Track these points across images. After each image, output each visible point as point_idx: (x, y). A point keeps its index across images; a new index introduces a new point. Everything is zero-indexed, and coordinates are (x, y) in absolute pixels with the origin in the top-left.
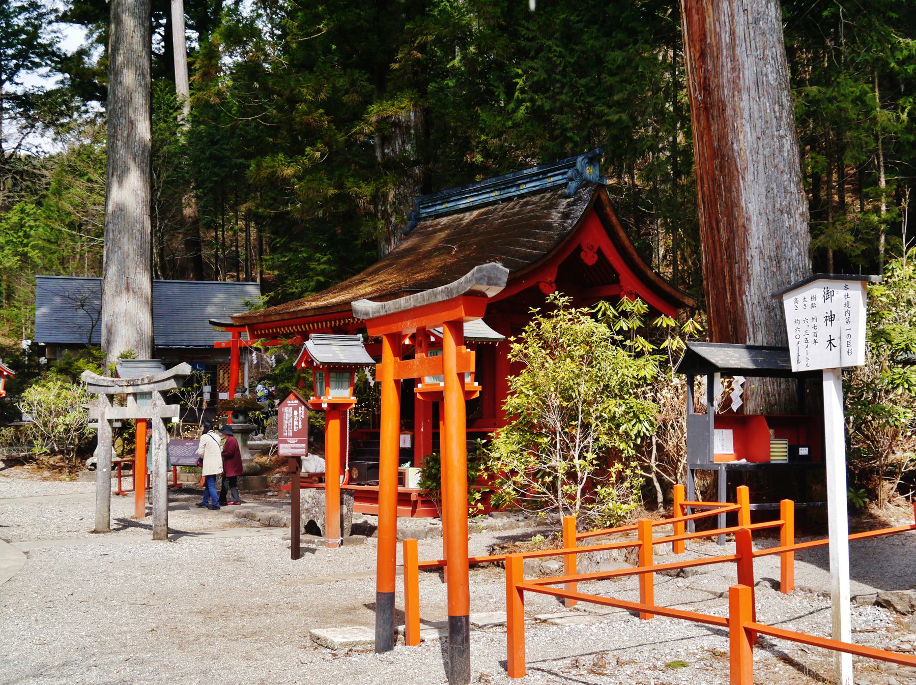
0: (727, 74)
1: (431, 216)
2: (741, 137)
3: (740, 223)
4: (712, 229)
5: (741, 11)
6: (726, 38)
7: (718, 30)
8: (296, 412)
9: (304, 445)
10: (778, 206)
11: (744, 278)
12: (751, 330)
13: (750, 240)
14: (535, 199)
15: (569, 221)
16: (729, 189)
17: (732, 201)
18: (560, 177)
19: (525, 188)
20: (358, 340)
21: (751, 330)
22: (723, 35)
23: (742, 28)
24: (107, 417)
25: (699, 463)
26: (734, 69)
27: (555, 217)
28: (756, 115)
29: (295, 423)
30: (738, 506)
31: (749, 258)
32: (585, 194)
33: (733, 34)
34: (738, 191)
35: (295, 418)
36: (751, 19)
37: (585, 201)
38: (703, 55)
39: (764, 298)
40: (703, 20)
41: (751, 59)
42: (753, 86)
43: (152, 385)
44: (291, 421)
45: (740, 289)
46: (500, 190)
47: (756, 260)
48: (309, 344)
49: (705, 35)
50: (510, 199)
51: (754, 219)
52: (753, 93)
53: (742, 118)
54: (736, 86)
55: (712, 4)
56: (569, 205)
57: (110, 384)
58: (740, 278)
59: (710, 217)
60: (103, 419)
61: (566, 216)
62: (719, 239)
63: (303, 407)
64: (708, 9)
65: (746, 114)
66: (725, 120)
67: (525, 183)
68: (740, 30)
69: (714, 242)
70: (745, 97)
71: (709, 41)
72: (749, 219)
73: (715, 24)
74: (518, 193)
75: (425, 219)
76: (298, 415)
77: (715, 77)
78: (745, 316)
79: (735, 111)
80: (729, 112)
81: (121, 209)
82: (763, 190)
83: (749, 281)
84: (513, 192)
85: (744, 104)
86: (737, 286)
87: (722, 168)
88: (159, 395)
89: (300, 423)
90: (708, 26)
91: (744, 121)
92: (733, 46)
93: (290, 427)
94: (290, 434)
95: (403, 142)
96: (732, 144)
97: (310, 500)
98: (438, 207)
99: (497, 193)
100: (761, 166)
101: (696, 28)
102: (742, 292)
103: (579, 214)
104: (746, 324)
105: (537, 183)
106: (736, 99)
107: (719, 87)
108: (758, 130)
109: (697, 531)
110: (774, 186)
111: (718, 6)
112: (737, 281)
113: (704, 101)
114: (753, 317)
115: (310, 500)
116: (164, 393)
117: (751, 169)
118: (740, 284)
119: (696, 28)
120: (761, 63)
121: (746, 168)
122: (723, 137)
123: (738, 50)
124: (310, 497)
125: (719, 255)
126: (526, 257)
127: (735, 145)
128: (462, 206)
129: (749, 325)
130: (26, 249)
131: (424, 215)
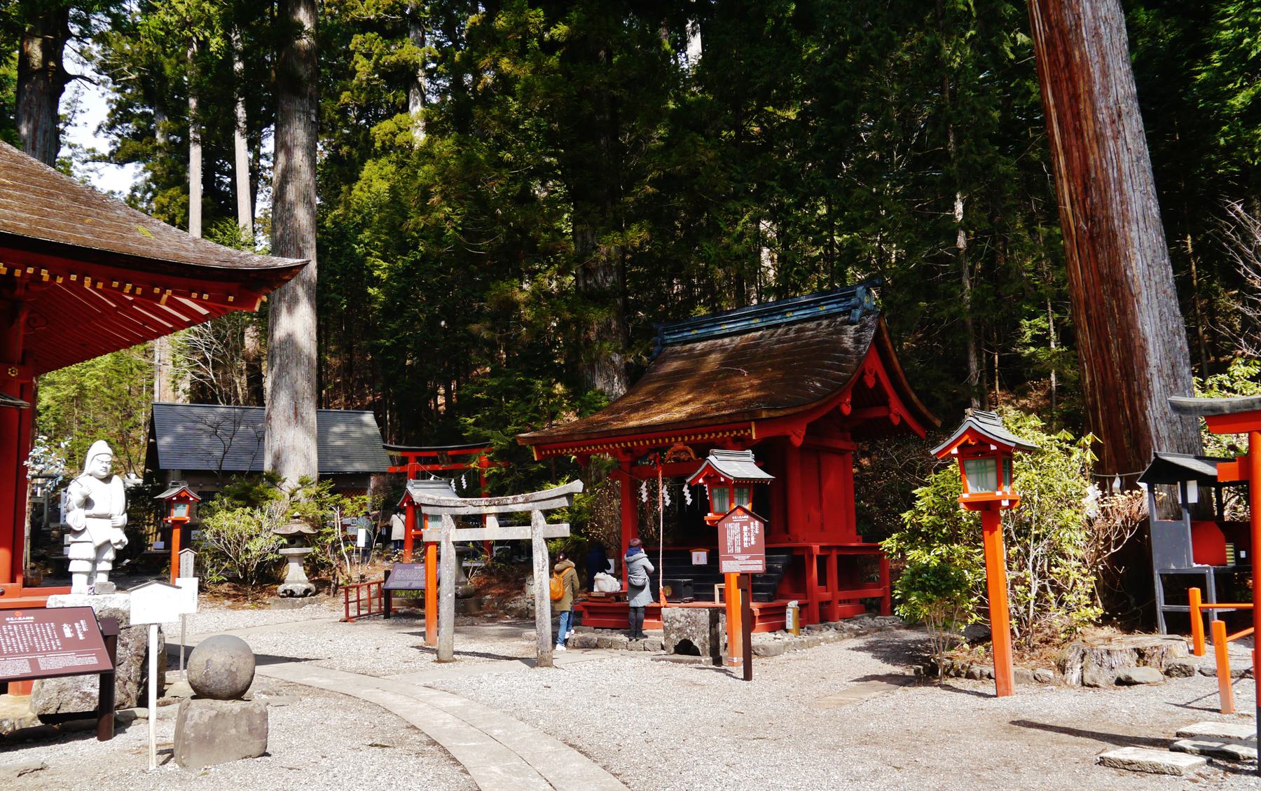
0: (1115, 207)
1: (678, 343)
2: (1133, 265)
3: (1137, 344)
4: (1101, 349)
5: (1125, 149)
6: (1113, 174)
7: (1105, 166)
8: (745, 528)
9: (760, 562)
10: (1170, 327)
11: (1145, 394)
12: (1155, 442)
13: (1148, 359)
14: (812, 325)
15: (862, 346)
16: (1123, 312)
17: (1128, 324)
18: (835, 306)
19: (791, 316)
20: (748, 455)
21: (1155, 442)
22: (1110, 171)
23: (1127, 165)
24: (452, 539)
25: (1173, 567)
26: (1122, 203)
27: (848, 342)
28: (1146, 244)
29: (746, 539)
30: (809, 600)
31: (1149, 376)
32: (870, 320)
33: (1119, 170)
34: (1133, 314)
35: (745, 534)
36: (1134, 159)
37: (871, 327)
38: (1086, 189)
39: (1166, 413)
40: (1086, 157)
41: (1137, 193)
42: (1140, 218)
43: (531, 504)
44: (738, 537)
45: (1141, 405)
46: (762, 317)
47: (1155, 378)
48: (711, 458)
49: (1088, 171)
50: (778, 326)
51: (1150, 340)
52: (1141, 224)
53: (1133, 247)
54: (1124, 216)
55: (1097, 142)
56: (857, 331)
57: (458, 504)
58: (1140, 394)
59: (1099, 339)
60: (447, 542)
61: (858, 341)
62: (1110, 358)
63: (757, 522)
64: (1091, 147)
65: (1136, 243)
66: (1117, 249)
67: (793, 311)
68: (1125, 167)
69: (1104, 361)
70: (1134, 227)
71: (1093, 175)
72: (1145, 340)
73: (1101, 161)
74: (785, 320)
75: (672, 345)
76: (749, 531)
77: (1103, 208)
78: (1148, 429)
79: (1126, 240)
80: (1120, 241)
81: (290, 340)
82: (1157, 314)
83: (1150, 397)
84: (778, 319)
85: (1134, 234)
86: (1137, 402)
87: (1114, 294)
88: (540, 514)
89: (753, 539)
90: (1092, 162)
91: (1135, 250)
92: (1120, 182)
93: (738, 543)
94: (738, 550)
95: (605, 275)
96: (1125, 270)
97: (683, 619)
98: (685, 334)
99: (758, 321)
100: (1154, 292)
101: (1076, 163)
102: (1143, 408)
103: (870, 339)
104: (1150, 437)
105: (808, 311)
106: (1126, 229)
107: (1109, 219)
108: (1149, 258)
109: (1168, 633)
110: (1165, 310)
111: (1103, 144)
112: (1137, 398)
113: (1090, 231)
114: (1157, 431)
115: (683, 619)
116: (547, 513)
117: (1145, 293)
118: (1141, 399)
119: (1076, 163)
120: (1145, 198)
121: (1140, 293)
122: (1114, 264)
123: (1125, 186)
124: (682, 616)
125: (1110, 374)
126: (837, 378)
127: (1128, 272)
128: (716, 333)
129: (1154, 438)
130: (83, 378)
131: (669, 341)
